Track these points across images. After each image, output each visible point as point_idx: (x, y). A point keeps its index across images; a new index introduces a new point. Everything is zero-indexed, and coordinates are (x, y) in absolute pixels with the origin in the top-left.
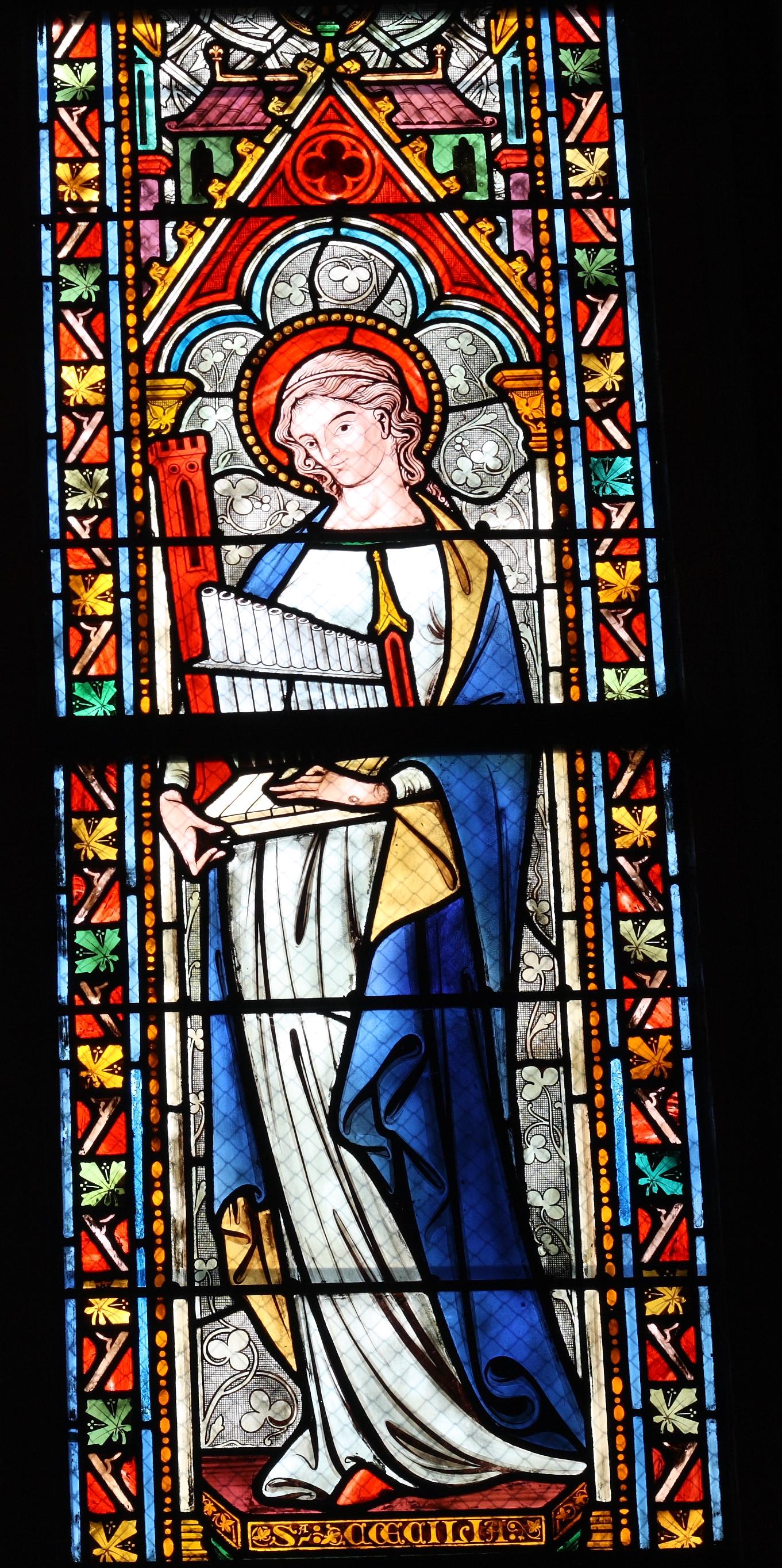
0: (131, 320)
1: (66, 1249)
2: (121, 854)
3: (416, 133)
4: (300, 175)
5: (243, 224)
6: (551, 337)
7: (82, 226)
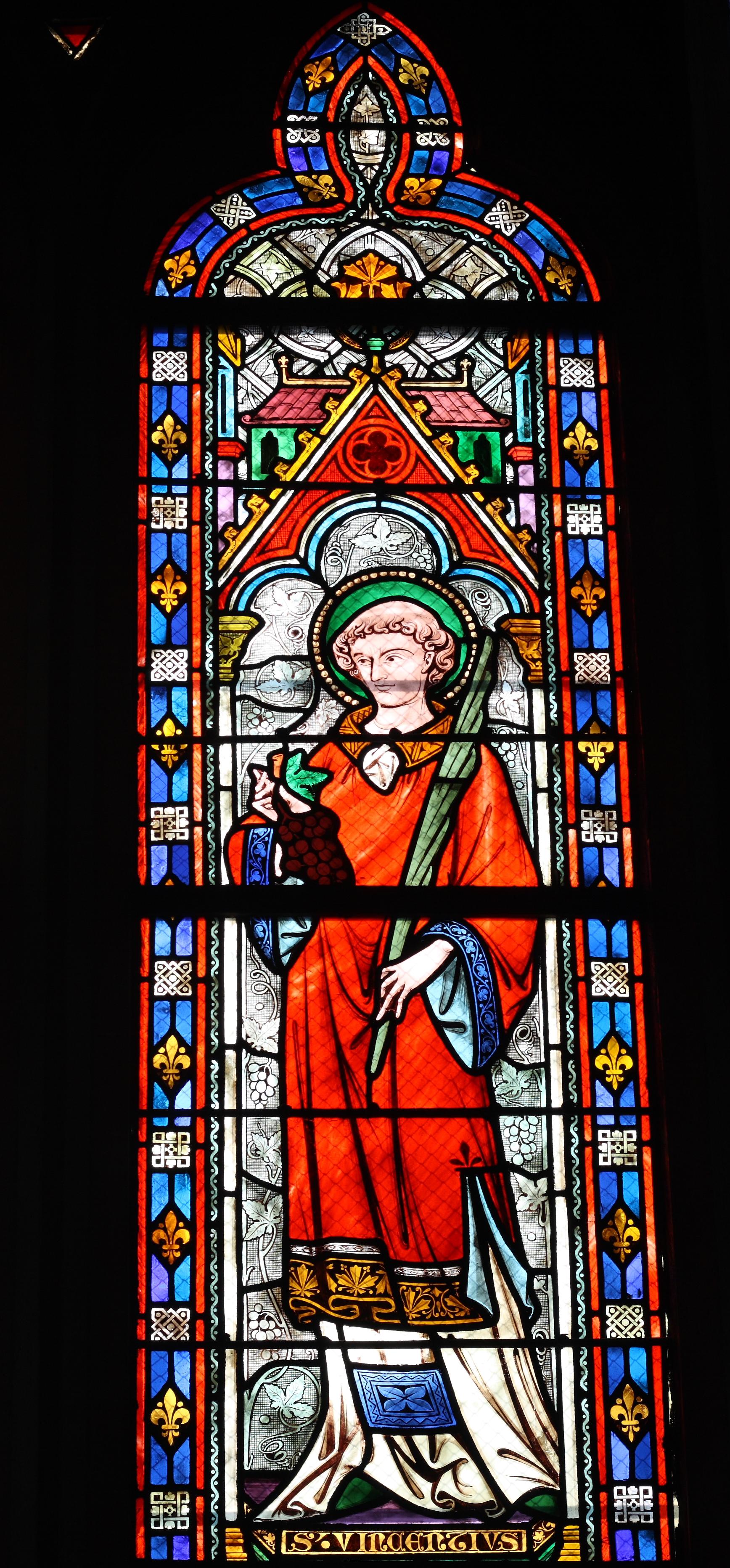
4: (348, 456)
5: (304, 495)
7: (338, 1247)
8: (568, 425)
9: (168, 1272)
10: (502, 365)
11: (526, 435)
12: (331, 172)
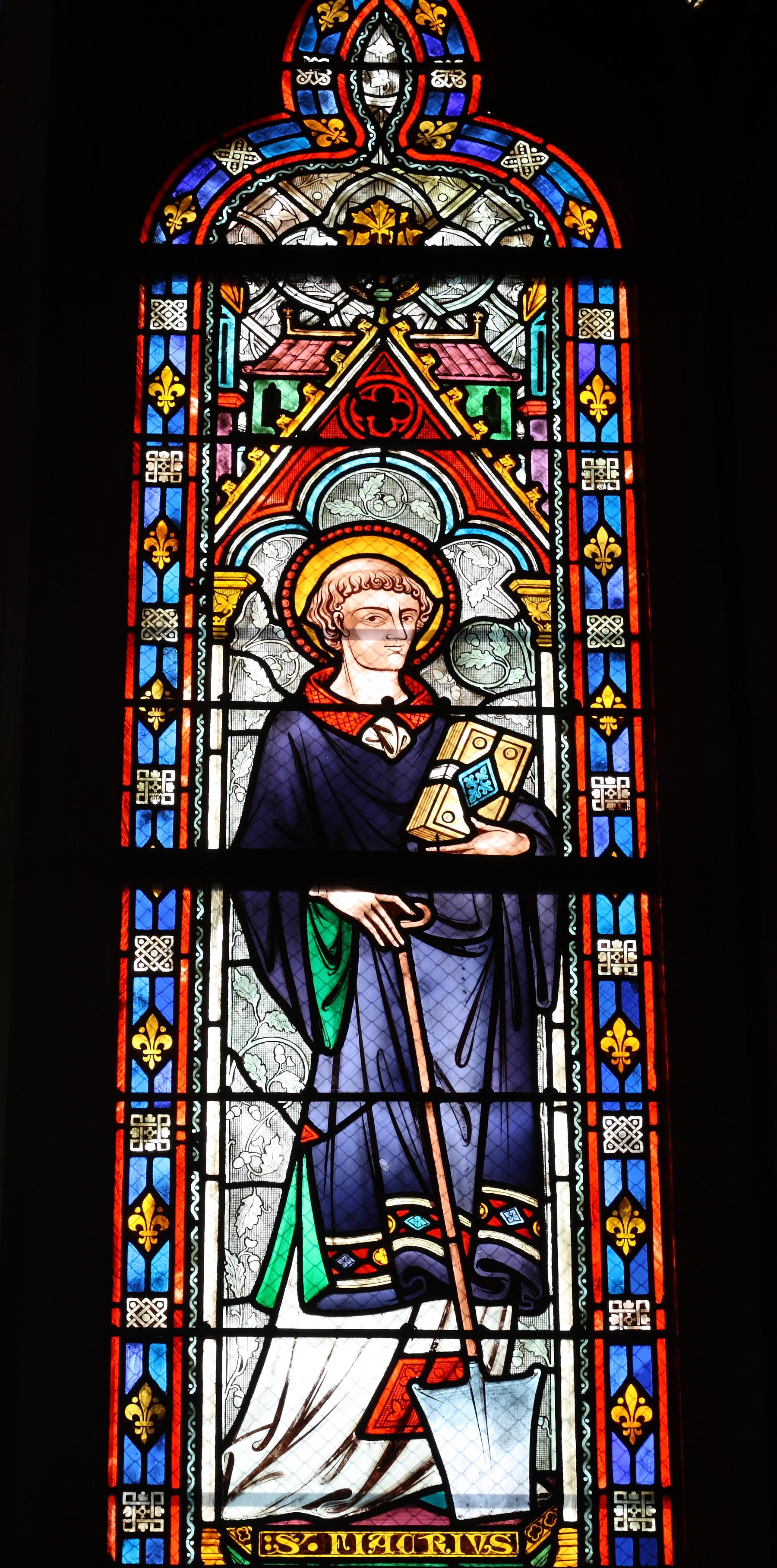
3: (453, 384)
8: (585, 378)
9: (156, 838)
10: (516, 317)
11: (540, 389)
12: (341, 116)
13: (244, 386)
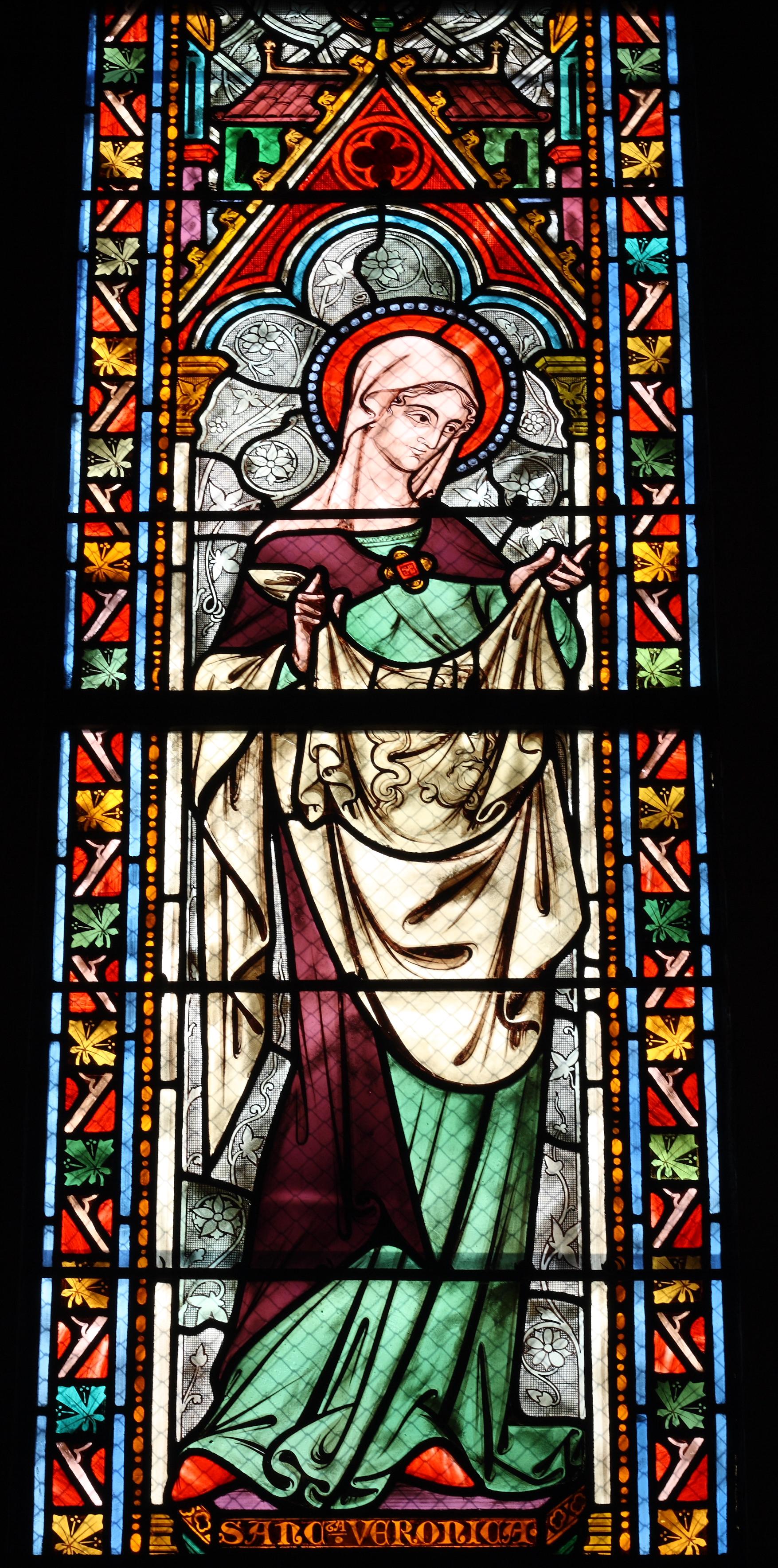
0: (167, 298)
1: (86, 116)
2: (146, 173)
6: (597, 323)
7: (121, 204)
13: (215, 136)
